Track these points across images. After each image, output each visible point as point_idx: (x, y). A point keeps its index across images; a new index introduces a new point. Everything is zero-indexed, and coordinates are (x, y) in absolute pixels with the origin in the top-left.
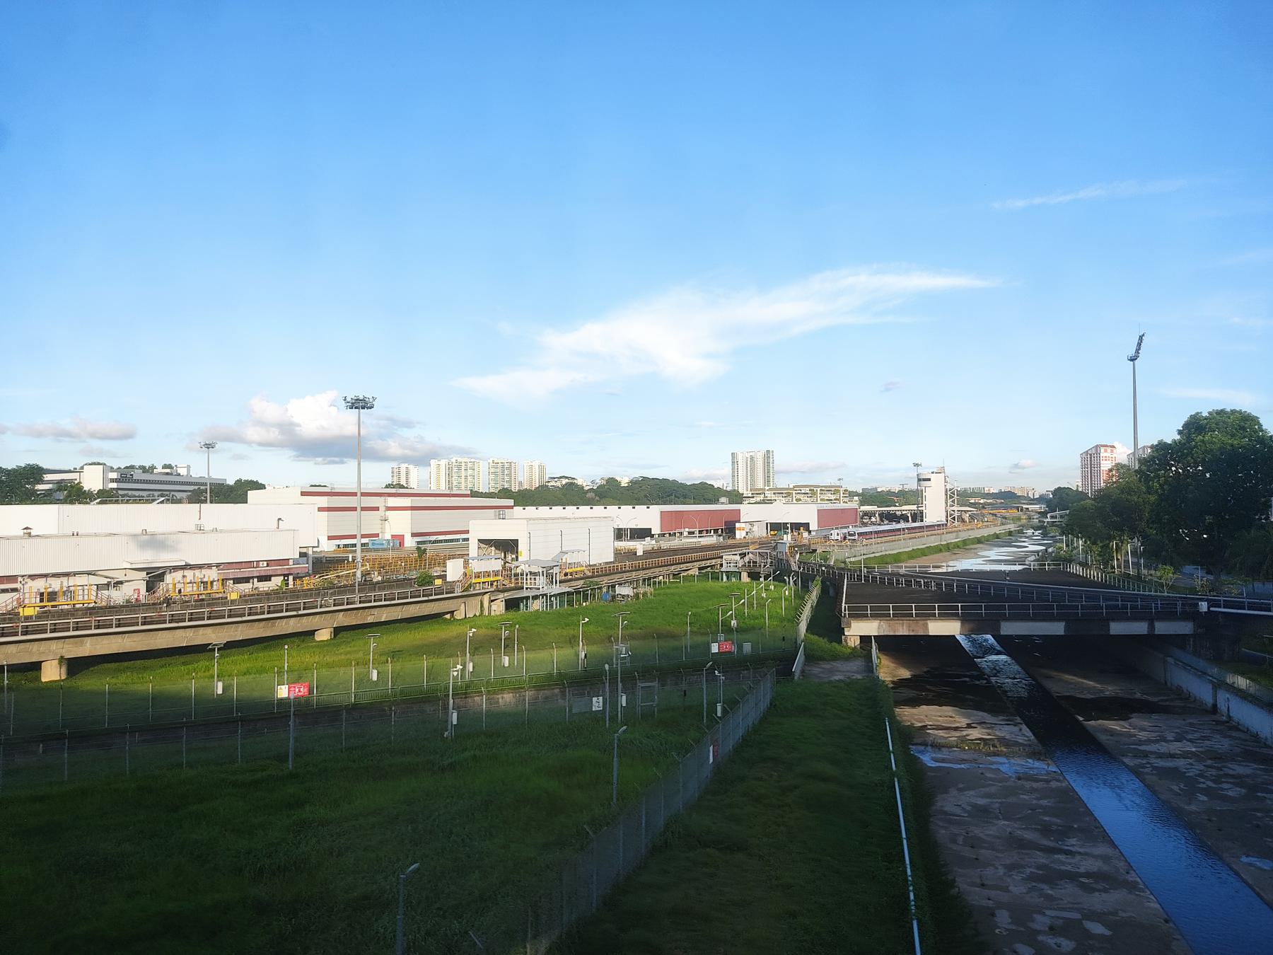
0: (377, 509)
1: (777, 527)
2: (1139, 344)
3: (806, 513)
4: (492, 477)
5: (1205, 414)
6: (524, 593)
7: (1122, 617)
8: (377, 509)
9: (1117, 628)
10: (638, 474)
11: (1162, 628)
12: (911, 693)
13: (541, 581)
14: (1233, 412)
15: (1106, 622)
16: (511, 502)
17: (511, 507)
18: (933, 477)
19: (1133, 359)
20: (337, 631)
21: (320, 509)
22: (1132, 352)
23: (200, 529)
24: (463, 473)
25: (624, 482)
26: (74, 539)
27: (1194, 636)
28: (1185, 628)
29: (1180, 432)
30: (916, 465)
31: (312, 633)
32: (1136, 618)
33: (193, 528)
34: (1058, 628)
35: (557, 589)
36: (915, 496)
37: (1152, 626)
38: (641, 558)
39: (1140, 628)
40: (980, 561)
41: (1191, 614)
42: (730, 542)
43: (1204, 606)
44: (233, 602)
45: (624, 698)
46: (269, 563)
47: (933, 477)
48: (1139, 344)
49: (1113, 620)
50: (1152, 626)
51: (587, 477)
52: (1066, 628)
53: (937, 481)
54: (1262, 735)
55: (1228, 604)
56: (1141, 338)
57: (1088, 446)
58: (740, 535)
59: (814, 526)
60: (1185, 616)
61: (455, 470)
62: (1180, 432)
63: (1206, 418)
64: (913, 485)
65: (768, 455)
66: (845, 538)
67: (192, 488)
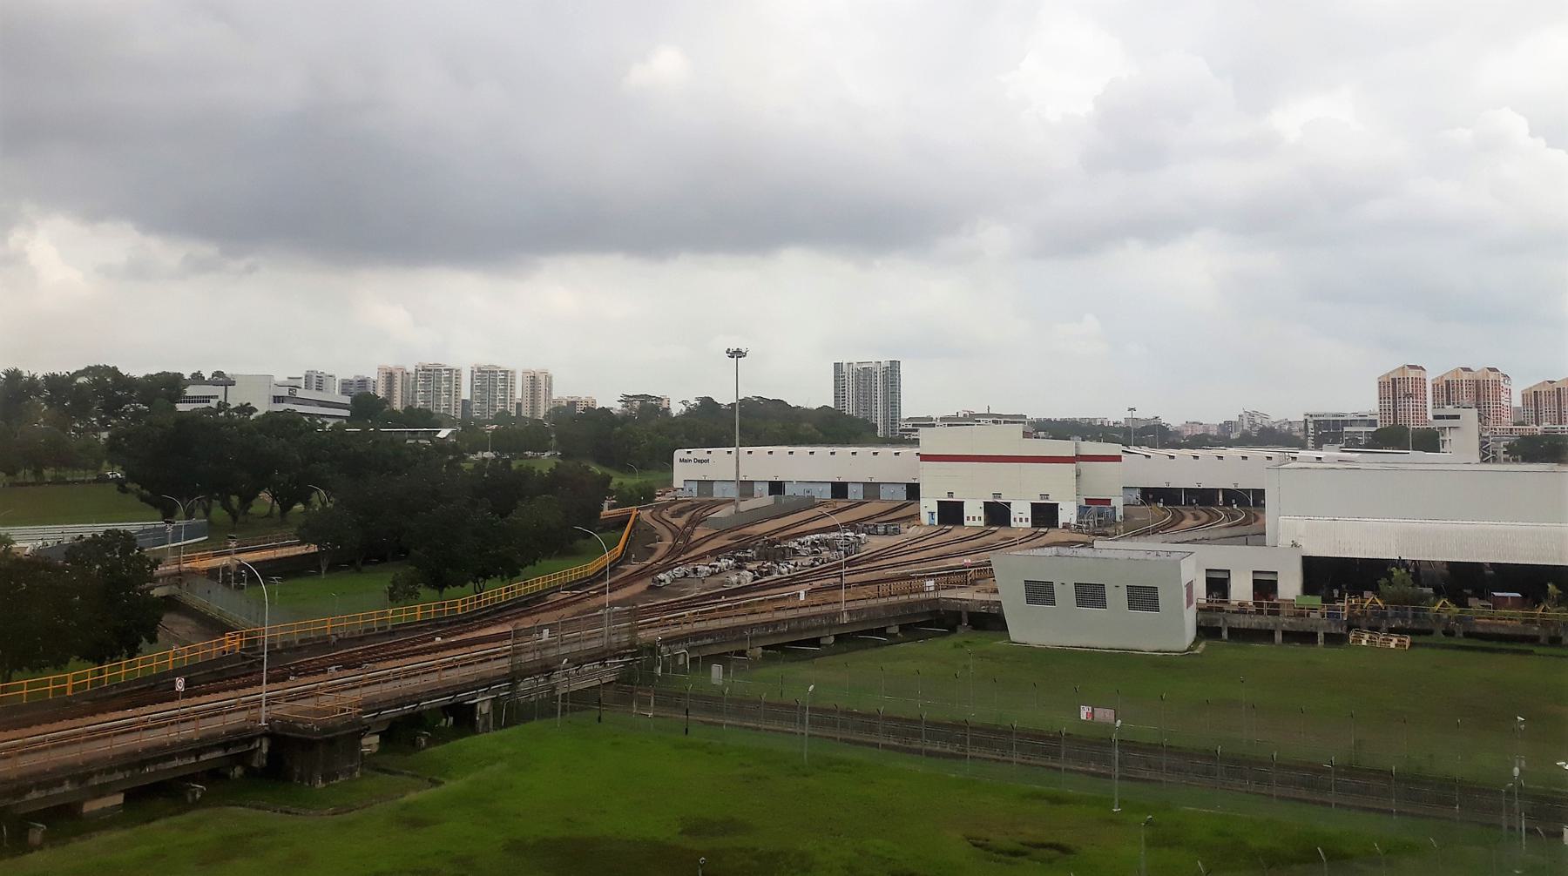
16: (1115, 449)
17: (1117, 459)
51: (1173, 419)
65: (893, 370)
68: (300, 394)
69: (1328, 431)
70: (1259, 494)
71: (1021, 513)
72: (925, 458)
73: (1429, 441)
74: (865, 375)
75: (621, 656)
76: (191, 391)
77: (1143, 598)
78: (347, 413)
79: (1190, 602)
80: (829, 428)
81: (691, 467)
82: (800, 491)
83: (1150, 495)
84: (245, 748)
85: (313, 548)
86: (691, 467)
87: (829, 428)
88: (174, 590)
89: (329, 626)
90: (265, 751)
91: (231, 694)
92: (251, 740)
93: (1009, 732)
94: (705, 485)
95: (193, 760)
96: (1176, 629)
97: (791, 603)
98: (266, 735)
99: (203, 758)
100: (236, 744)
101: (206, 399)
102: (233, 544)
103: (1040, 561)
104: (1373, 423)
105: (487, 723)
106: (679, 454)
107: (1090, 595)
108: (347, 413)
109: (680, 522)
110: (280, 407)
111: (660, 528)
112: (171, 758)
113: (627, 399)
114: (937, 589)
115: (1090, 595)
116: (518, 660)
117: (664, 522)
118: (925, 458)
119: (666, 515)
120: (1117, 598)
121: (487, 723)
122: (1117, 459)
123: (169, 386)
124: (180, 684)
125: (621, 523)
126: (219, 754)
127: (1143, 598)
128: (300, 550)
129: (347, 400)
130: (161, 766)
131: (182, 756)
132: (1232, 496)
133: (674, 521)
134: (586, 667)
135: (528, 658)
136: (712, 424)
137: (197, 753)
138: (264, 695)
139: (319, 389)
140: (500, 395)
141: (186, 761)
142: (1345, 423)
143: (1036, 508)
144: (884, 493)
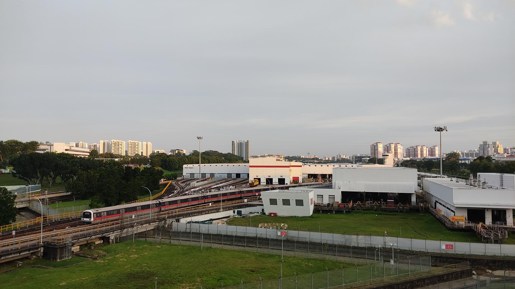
4: (130, 149)
17: (301, 166)
61: (113, 145)
65: (247, 144)
68: (73, 148)
69: (359, 160)
70: (331, 176)
71: (275, 181)
72: (250, 166)
73: (381, 162)
74: (240, 145)
75: (155, 222)
76: (41, 147)
77: (299, 203)
78: (89, 154)
79: (312, 204)
80: (229, 158)
81: (188, 169)
82: (218, 176)
83: (310, 176)
84: (36, 251)
85: (69, 193)
86: (188, 169)
87: (229, 158)
88: (28, 205)
89: (69, 215)
90: (42, 251)
91: (35, 235)
92: (37, 248)
93: (349, 247)
94: (192, 175)
95: (18, 255)
96: (310, 210)
97: (208, 206)
98: (42, 246)
99: (21, 254)
100: (32, 249)
101: (45, 150)
102: (46, 192)
103: (278, 194)
104: (369, 157)
105: (113, 242)
106: (185, 166)
107: (286, 202)
108: (89, 154)
109: (183, 185)
110: (66, 152)
111: (177, 187)
112: (11, 254)
113: (172, 151)
114: (248, 202)
115: (286, 202)
116: (122, 224)
117: (178, 185)
118: (250, 166)
119: (179, 183)
120: (293, 203)
121: (113, 242)
122: (301, 166)
123: (34, 145)
124: (14, 233)
125: (165, 185)
126: (28, 252)
127: (299, 203)
128: (65, 194)
129: (88, 150)
130: (7, 257)
131: (14, 253)
132: (324, 176)
133: (181, 185)
134: (144, 225)
135: (125, 223)
136: (195, 158)
137: (20, 252)
138: (42, 236)
139: (82, 147)
140: (136, 149)
141: (16, 255)
142: (363, 157)
143: (267, 180)
144: (241, 176)
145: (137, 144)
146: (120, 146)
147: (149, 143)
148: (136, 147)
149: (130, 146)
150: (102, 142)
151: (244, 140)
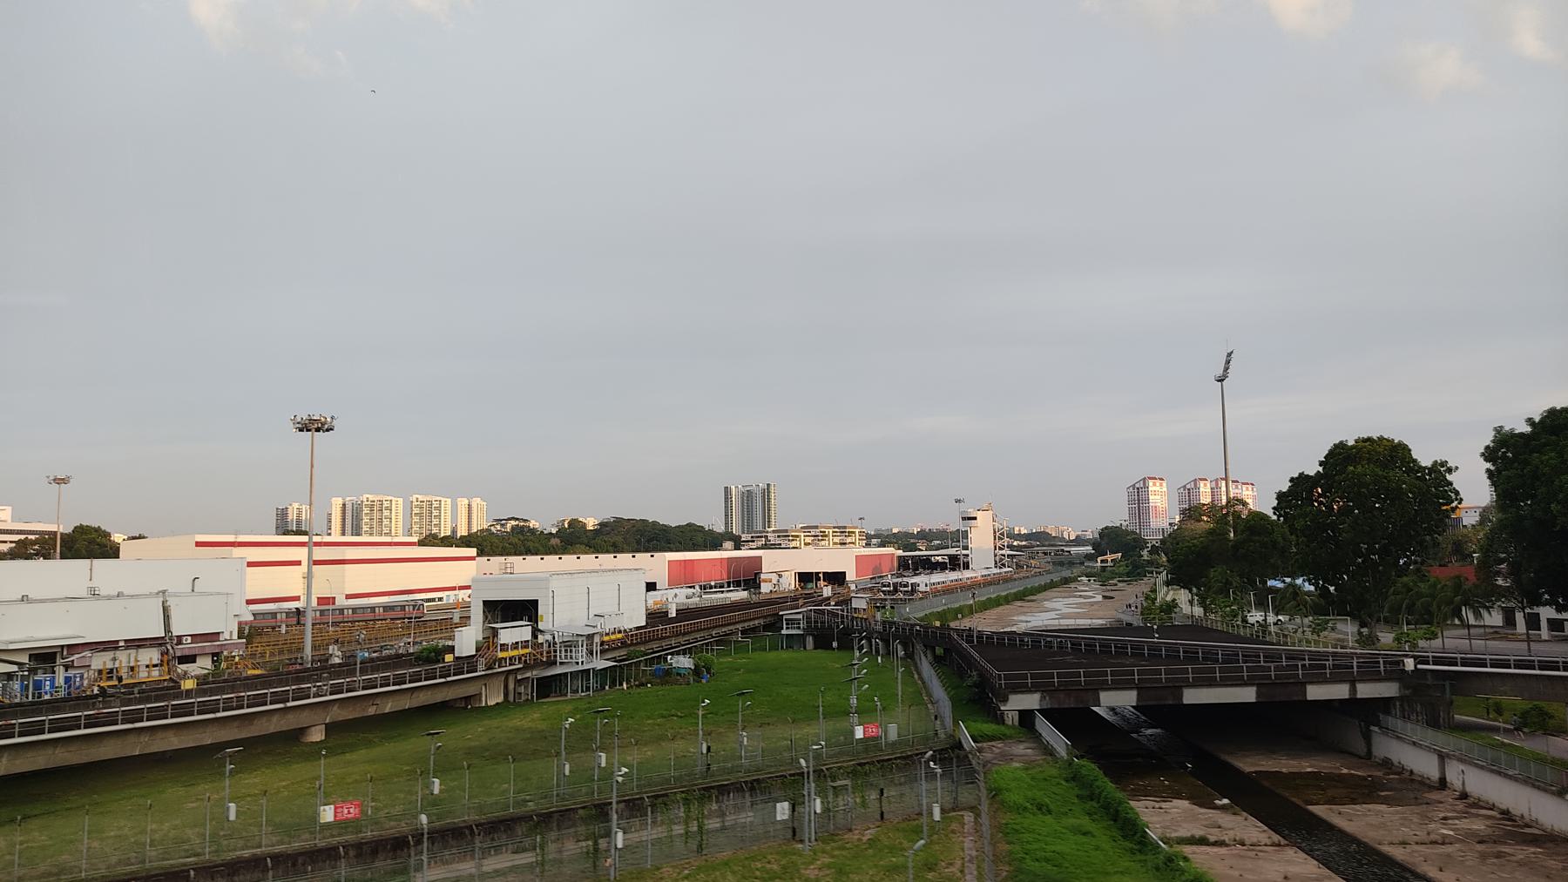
0: (298, 563)
1: (805, 578)
2: (1228, 362)
3: (842, 559)
5: (1351, 443)
6: (558, 670)
7: (1322, 680)
8: (298, 563)
9: (1315, 692)
10: (608, 514)
11: (1366, 690)
12: (1549, 775)
13: (581, 654)
14: (1381, 439)
15: (1177, 690)
16: (473, 552)
17: (472, 558)
18: (979, 515)
19: (1221, 381)
20: (330, 728)
21: (250, 564)
22: (1220, 372)
23: (94, 594)
24: (376, 515)
25: (591, 523)
26: (24, 606)
27: (1401, 698)
28: (1388, 690)
29: (1321, 464)
30: (958, 501)
31: (302, 731)
32: (1335, 679)
33: (84, 593)
34: (1248, 695)
35: (601, 664)
36: (960, 537)
37: (1353, 690)
38: (672, 620)
39: (1340, 691)
40: (1052, 615)
41: (1394, 672)
42: (755, 598)
43: (1410, 664)
44: (189, 693)
45: (818, 801)
46: (196, 637)
47: (979, 515)
48: (1228, 362)
49: (1311, 683)
50: (1353, 690)
51: (544, 521)
52: (1258, 694)
53: (984, 519)
54: (1515, 811)
55: (1437, 661)
56: (1229, 355)
57: (1136, 478)
58: (765, 588)
59: (851, 576)
60: (1388, 677)
61: (366, 510)
62: (1321, 464)
63: (1352, 447)
64: (955, 525)
65: (766, 492)
66: (896, 590)
67: (16, 538)
74: (748, 497)
122: (472, 558)
140: (435, 521)
145: (435, 504)
146: (386, 513)
147: (476, 502)
148: (435, 513)
149: (416, 511)
150: (337, 502)
151: (757, 482)
